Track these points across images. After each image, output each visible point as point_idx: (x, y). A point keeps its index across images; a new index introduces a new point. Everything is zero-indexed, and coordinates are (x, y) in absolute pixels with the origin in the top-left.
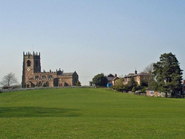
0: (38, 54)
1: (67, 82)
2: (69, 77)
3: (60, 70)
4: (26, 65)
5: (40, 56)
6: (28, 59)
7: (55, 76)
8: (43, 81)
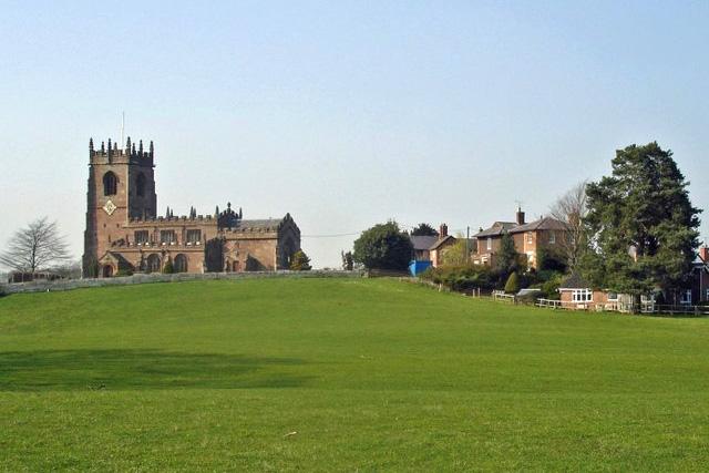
0: (146, 149)
1: (257, 254)
2: (267, 235)
3: (229, 210)
4: (100, 189)
5: (152, 154)
6: (109, 168)
7: (211, 234)
8: (164, 253)
